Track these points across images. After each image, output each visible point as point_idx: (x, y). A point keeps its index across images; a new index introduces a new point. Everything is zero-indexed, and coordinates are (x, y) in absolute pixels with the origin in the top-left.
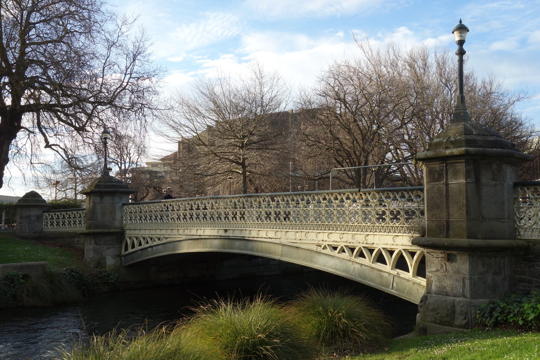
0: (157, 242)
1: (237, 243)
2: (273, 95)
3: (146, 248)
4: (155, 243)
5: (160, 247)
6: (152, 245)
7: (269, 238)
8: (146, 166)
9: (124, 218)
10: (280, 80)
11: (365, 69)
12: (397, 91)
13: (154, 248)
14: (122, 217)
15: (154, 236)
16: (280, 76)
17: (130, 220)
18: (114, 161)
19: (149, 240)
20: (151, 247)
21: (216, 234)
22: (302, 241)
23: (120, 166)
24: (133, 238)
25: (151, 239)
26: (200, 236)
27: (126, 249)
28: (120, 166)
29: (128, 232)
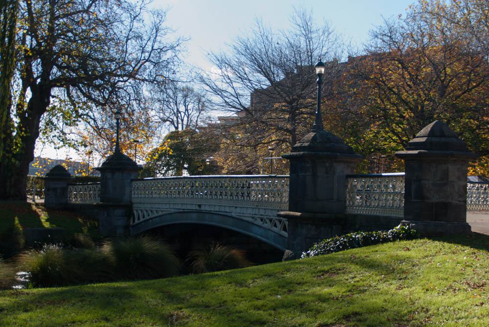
0: (156, 215)
1: (216, 217)
2: (323, 52)
3: (148, 220)
4: (154, 216)
5: (157, 219)
6: (152, 217)
7: (226, 212)
8: (219, 122)
9: (133, 193)
10: (331, 36)
11: (406, 27)
12: (312, 87)
13: (154, 219)
14: (131, 192)
15: (265, 217)
16: (330, 30)
17: (215, 195)
18: (169, 119)
19: (150, 212)
20: (151, 219)
21: (194, 208)
22: (244, 215)
23: (176, 126)
24: (276, 221)
25: (151, 211)
26: (184, 209)
27: (134, 221)
28: (176, 126)
29: (135, 206)
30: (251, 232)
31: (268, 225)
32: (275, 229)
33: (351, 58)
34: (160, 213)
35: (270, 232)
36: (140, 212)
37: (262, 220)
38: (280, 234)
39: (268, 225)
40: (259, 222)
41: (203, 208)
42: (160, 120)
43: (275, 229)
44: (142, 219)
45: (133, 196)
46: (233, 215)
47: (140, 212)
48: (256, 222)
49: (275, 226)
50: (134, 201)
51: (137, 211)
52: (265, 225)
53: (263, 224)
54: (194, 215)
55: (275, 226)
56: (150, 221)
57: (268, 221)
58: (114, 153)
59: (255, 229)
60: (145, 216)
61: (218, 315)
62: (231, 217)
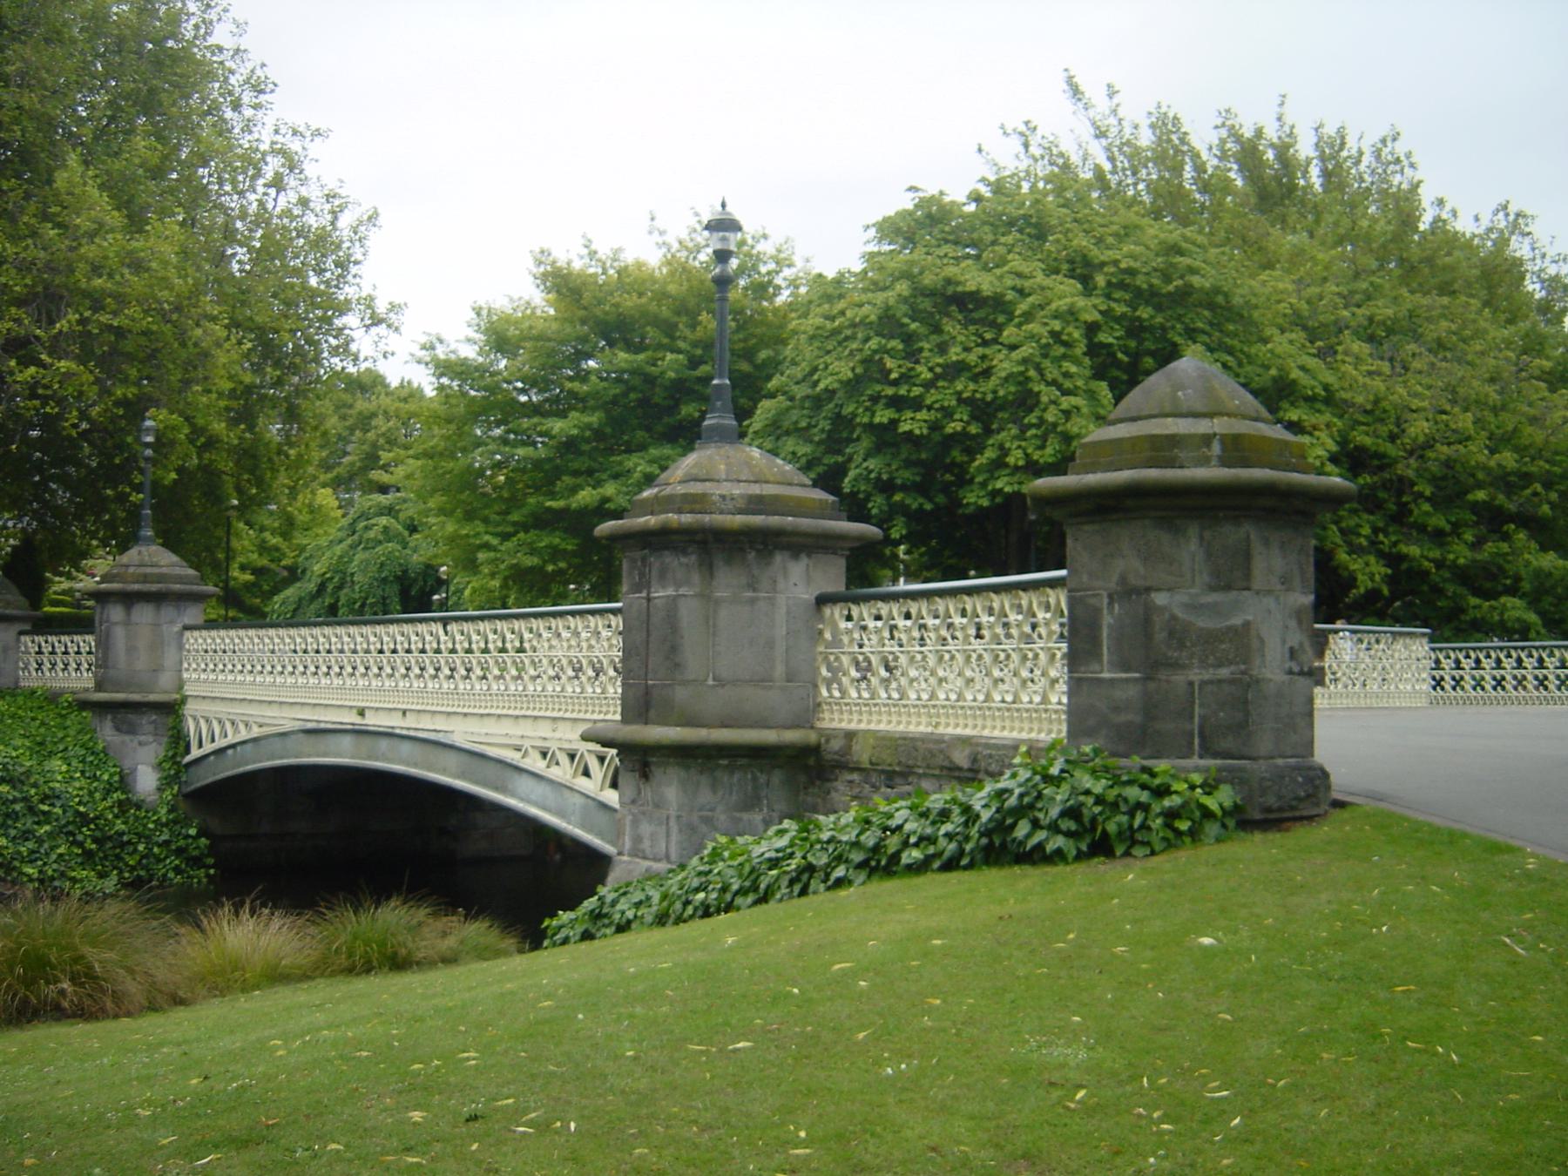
0: (244, 734)
5: (249, 747)
19: (228, 725)
20: (233, 746)
29: (190, 708)
30: (513, 795)
31: (563, 772)
32: (582, 783)
33: (402, 386)
34: (256, 732)
35: (567, 793)
36: (215, 724)
37: (544, 755)
38: (601, 799)
39: (563, 772)
40: (536, 763)
41: (373, 721)
42: (1290, 312)
43: (582, 783)
44: (208, 747)
45: (185, 675)
46: (459, 740)
47: (215, 724)
48: (527, 763)
49: (586, 773)
50: (189, 690)
51: (195, 718)
52: (555, 773)
53: (548, 767)
54: (347, 741)
55: (586, 773)
56: (230, 752)
57: (563, 759)
58: (559, 479)
59: (524, 784)
60: (217, 738)
61: (1458, 938)
62: (451, 747)
